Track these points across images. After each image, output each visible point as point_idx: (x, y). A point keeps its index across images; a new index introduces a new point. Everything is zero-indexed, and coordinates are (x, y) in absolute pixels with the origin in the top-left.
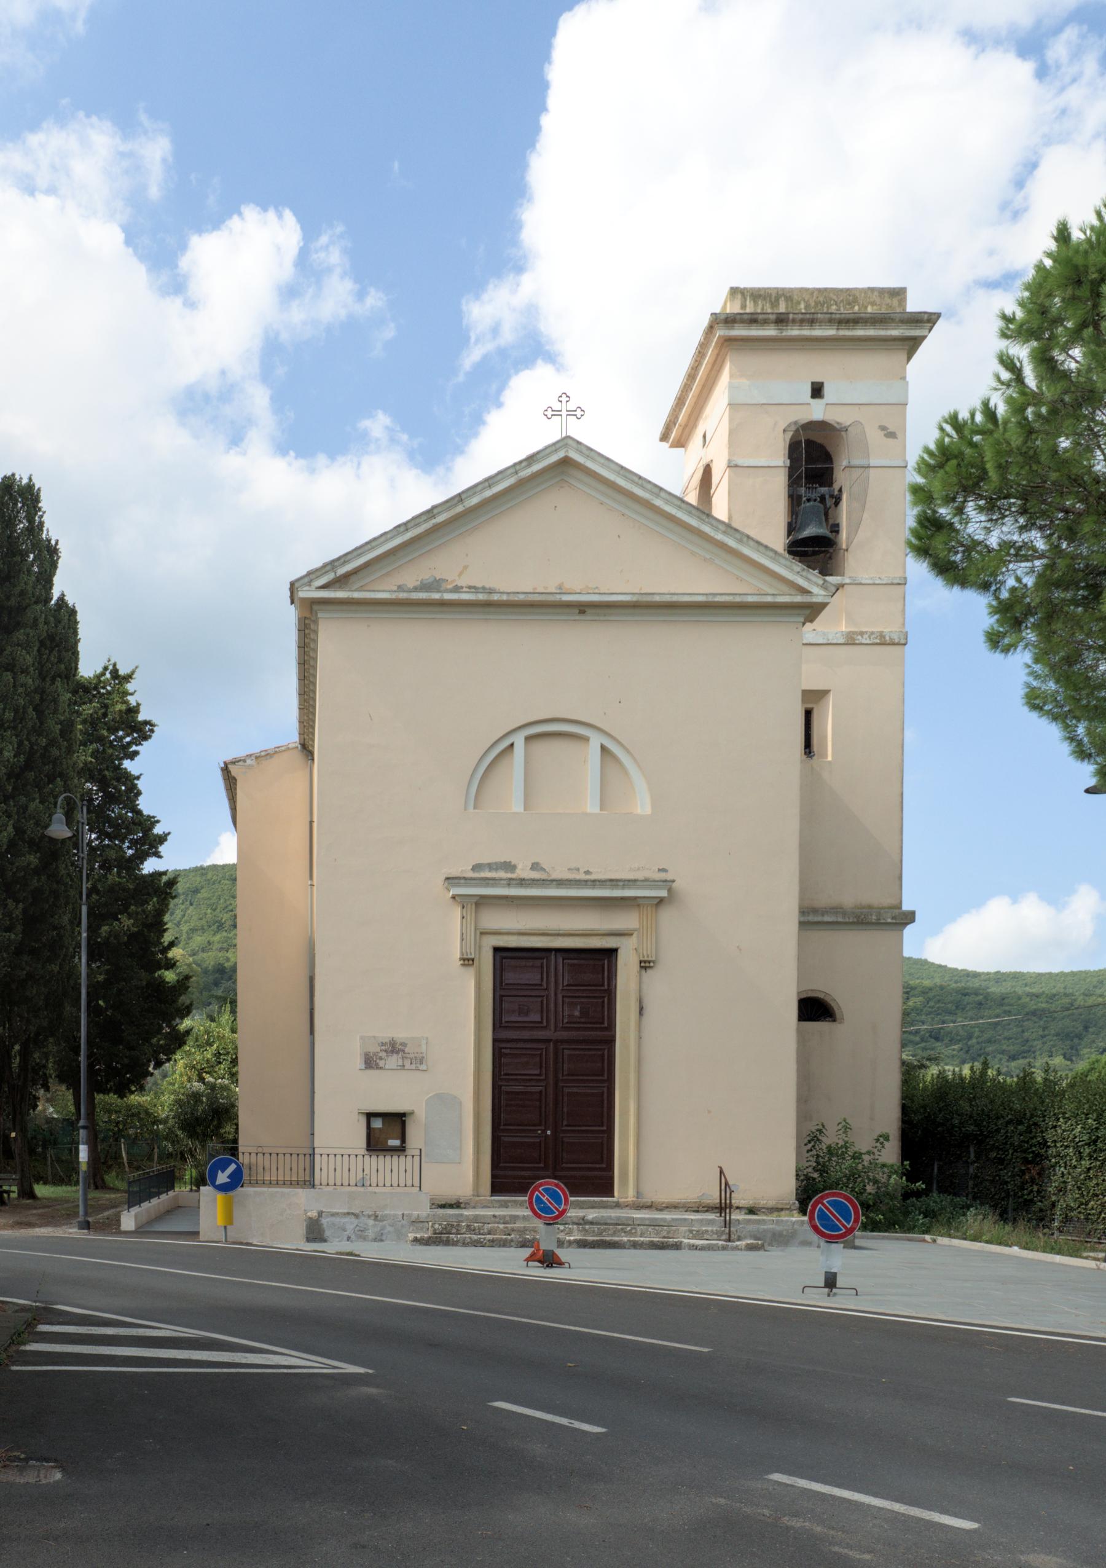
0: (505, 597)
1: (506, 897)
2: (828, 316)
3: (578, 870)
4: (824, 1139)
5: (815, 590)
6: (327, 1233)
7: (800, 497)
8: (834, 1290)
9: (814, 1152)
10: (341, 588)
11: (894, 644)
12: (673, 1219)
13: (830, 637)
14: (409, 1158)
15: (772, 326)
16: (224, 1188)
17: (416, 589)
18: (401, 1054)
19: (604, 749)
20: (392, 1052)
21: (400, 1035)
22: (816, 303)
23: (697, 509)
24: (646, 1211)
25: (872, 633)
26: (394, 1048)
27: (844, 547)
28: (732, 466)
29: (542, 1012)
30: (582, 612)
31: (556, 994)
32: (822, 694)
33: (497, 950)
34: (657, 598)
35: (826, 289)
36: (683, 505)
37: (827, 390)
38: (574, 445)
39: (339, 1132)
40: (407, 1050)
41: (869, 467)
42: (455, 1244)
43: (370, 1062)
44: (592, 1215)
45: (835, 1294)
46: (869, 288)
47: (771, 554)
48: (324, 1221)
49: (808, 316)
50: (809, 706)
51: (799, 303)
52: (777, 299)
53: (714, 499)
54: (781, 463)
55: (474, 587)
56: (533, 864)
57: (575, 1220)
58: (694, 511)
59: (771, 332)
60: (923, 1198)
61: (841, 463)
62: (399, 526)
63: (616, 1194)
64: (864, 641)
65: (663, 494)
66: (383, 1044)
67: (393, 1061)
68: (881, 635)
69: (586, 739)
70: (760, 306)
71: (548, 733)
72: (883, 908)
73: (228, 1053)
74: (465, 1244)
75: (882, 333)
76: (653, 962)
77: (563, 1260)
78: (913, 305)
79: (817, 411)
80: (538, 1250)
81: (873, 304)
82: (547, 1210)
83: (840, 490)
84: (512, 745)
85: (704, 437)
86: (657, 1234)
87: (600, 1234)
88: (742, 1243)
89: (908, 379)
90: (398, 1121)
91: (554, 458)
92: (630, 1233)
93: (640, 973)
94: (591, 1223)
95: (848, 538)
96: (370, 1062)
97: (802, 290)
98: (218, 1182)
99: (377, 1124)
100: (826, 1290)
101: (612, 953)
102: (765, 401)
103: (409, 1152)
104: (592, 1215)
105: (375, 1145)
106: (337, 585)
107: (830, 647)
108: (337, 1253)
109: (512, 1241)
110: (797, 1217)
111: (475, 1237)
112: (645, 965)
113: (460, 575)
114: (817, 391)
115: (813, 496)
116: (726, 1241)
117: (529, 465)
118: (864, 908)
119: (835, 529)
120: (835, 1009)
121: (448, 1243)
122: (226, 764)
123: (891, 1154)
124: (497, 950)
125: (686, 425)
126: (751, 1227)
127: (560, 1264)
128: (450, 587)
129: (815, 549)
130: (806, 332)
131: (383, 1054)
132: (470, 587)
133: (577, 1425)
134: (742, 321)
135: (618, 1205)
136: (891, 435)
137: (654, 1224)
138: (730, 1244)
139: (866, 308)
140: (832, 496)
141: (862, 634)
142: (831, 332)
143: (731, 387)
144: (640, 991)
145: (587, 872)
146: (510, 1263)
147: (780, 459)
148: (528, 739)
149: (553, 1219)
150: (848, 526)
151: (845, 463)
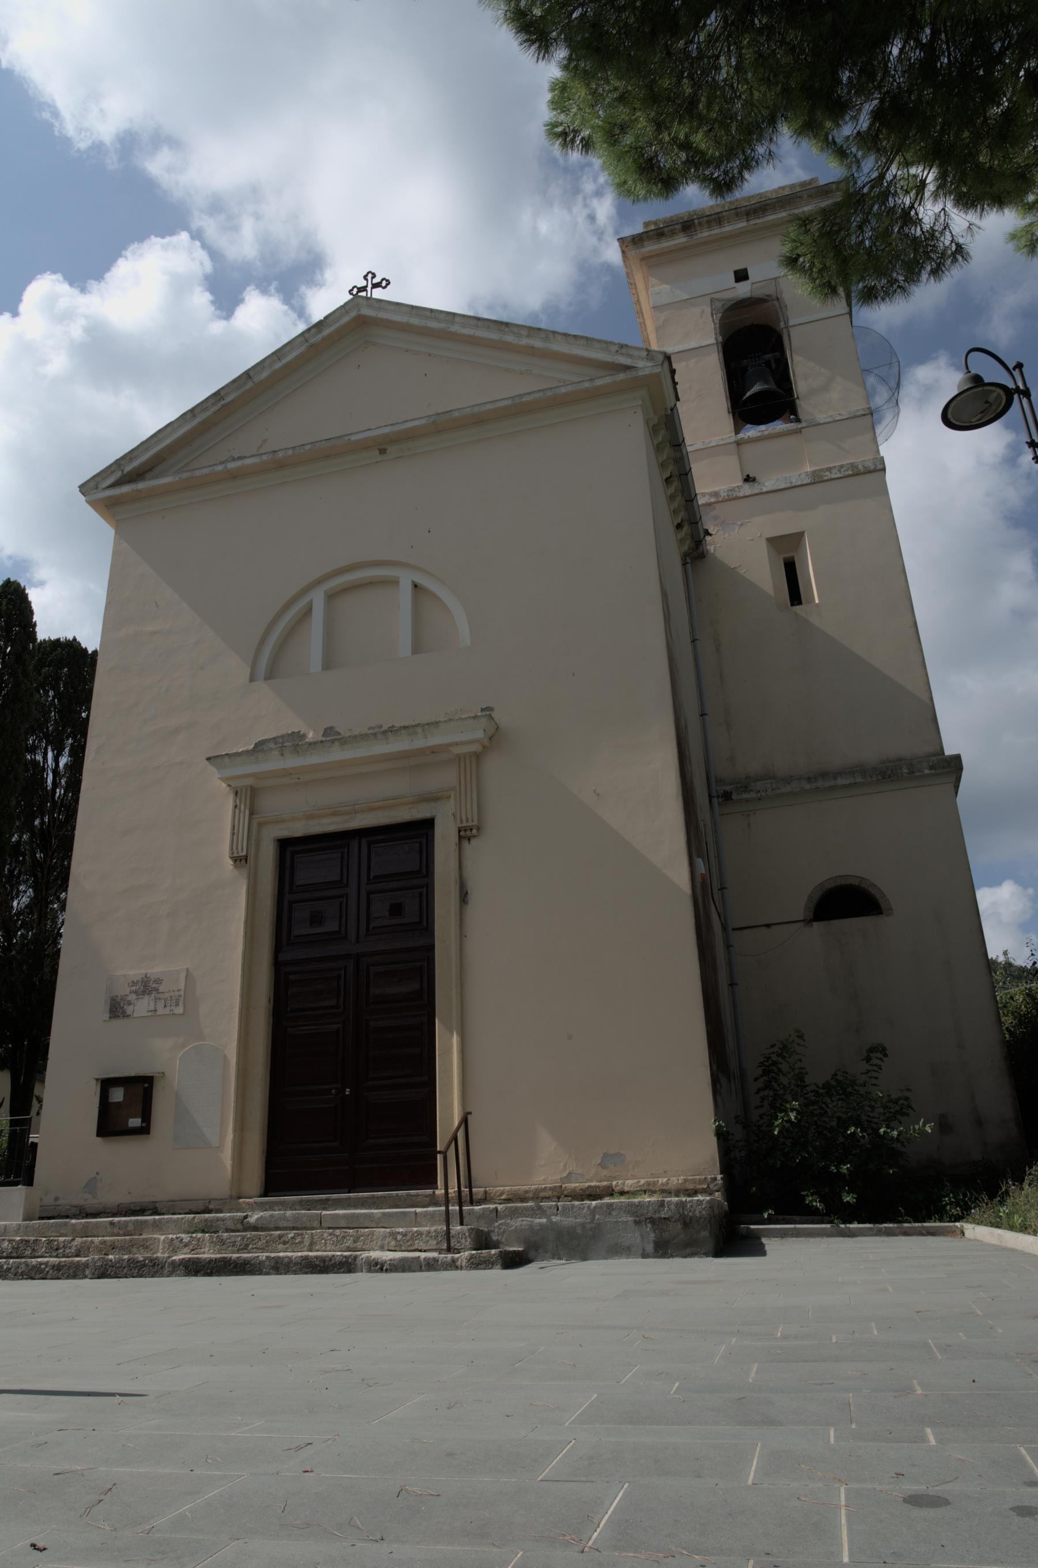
5: (640, 364)
11: (870, 472)
13: (794, 480)
15: (681, 235)
20: (144, 993)
21: (156, 970)
25: (842, 466)
30: (383, 451)
32: (797, 538)
36: (480, 323)
40: (161, 989)
54: (712, 341)
59: (681, 240)
64: (833, 476)
66: (134, 983)
68: (853, 466)
69: (394, 582)
71: (352, 584)
79: (743, 290)
92: (293, 1244)
94: (255, 1228)
99: (117, 1095)
101: (428, 824)
102: (687, 297)
107: (795, 490)
109: (86, 1265)
112: (465, 835)
117: (320, 332)
120: (878, 896)
131: (132, 997)
134: (649, 238)
141: (829, 469)
142: (743, 224)
148: (331, 597)
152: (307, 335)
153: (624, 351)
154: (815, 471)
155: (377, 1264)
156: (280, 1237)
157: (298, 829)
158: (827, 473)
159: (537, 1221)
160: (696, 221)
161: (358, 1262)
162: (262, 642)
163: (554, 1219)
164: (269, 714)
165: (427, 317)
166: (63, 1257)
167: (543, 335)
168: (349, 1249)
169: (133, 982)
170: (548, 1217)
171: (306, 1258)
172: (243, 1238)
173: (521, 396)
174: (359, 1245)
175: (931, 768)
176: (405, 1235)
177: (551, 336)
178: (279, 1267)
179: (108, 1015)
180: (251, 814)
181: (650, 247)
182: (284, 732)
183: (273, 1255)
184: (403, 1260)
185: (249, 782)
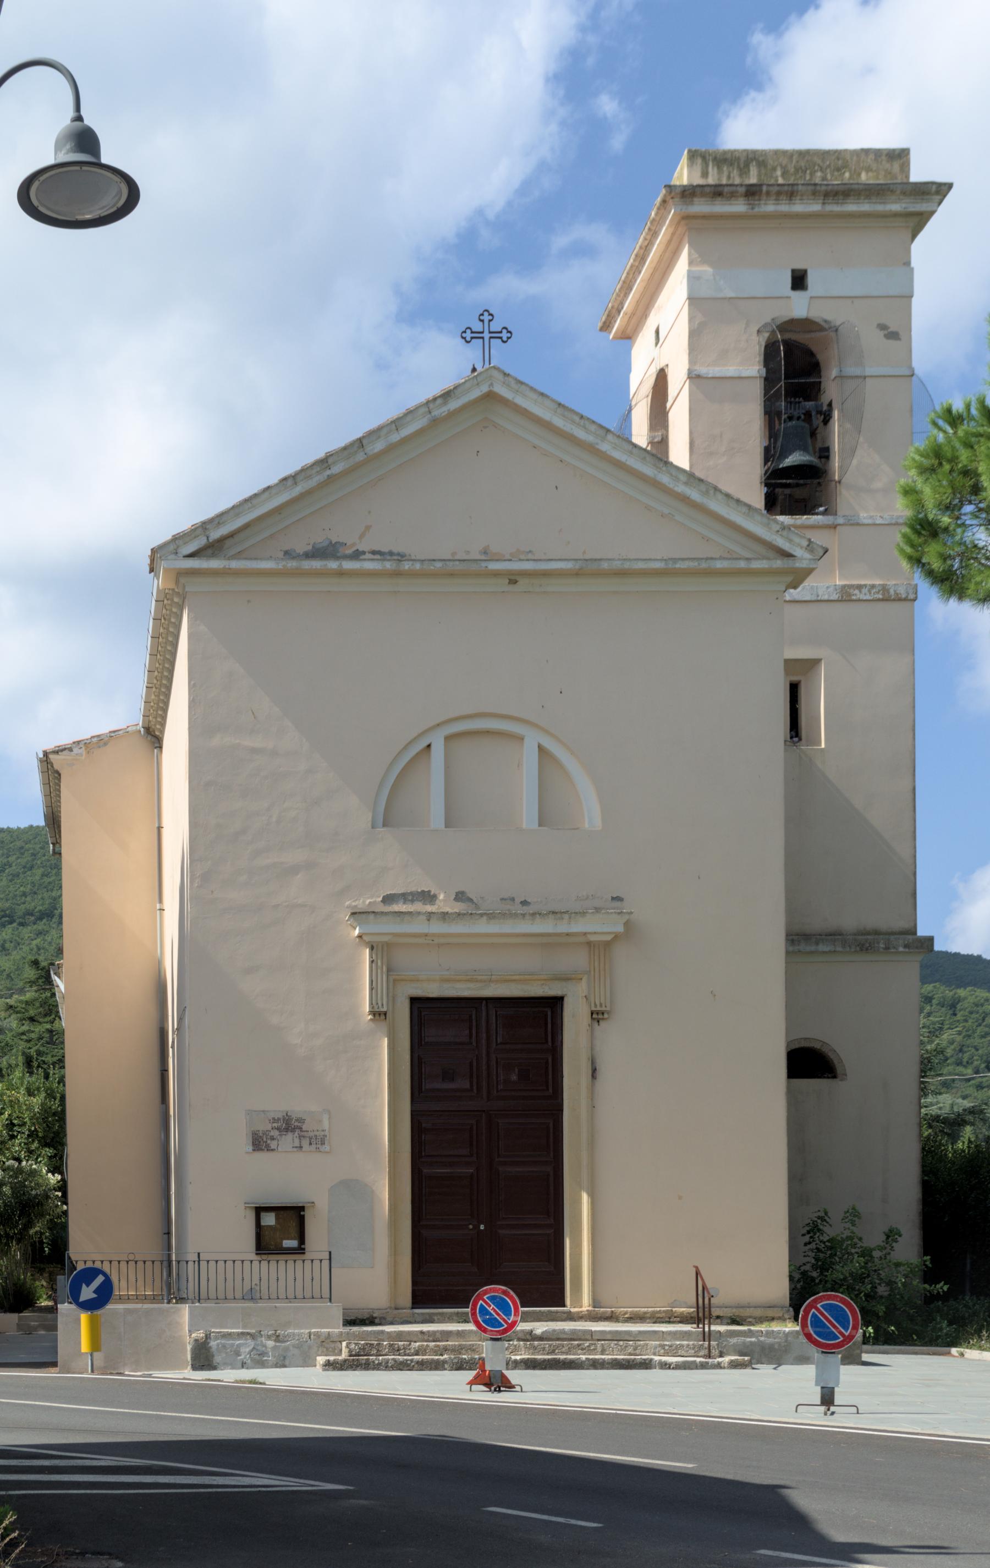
0: (418, 566)
1: (553, 1078)
2: (810, 188)
3: (513, 899)
4: (826, 1229)
5: (798, 552)
6: (218, 1359)
7: (779, 414)
8: (832, 1409)
9: (813, 1246)
10: (213, 556)
11: (900, 600)
12: (640, 1332)
14: (308, 1263)
15: (741, 200)
16: (89, 1306)
17: (308, 556)
18: (297, 1132)
19: (540, 748)
20: (287, 1130)
22: (797, 170)
23: (653, 455)
24: (606, 1323)
25: (873, 586)
26: (289, 1125)
27: (837, 478)
28: (694, 377)
29: (471, 1076)
30: (513, 582)
31: (488, 1054)
33: (414, 1001)
34: (605, 565)
35: (808, 152)
37: (811, 279)
38: (501, 377)
39: (217, 1230)
41: (865, 377)
42: (377, 1367)
43: (259, 1143)
44: (540, 1328)
45: (833, 1413)
46: (862, 150)
47: (744, 509)
48: (213, 1344)
49: (786, 188)
50: (795, 678)
51: (774, 169)
52: (747, 165)
53: (670, 415)
55: (379, 553)
56: (457, 894)
57: (520, 1335)
58: (648, 458)
59: (739, 207)
60: (952, 1302)
61: (831, 373)
62: (285, 479)
63: (568, 1301)
64: (862, 597)
65: (610, 437)
66: (275, 1120)
67: (288, 1140)
68: (884, 588)
69: (521, 739)
70: (726, 174)
71: (475, 734)
72: (893, 933)
73: (24, 1124)
74: (387, 1367)
75: (880, 208)
76: (608, 1013)
77: (513, 1382)
78: (916, 175)
79: (798, 306)
80: (484, 1371)
81: (868, 169)
82: (493, 1322)
83: (830, 405)
84: (429, 746)
85: (657, 332)
86: (623, 1350)
87: (553, 1352)
88: (726, 1359)
89: (913, 265)
90: (294, 1216)
91: (476, 394)
92: (588, 1350)
93: (591, 1026)
95: (840, 467)
96: (259, 1143)
97: (777, 153)
98: (82, 1299)
99: (269, 1220)
100: (823, 1408)
101: (556, 1003)
102: (732, 295)
103: (308, 1255)
104: (540, 1328)
105: (265, 1245)
106: (210, 551)
108: (236, 1382)
109: (444, 1362)
110: (791, 1327)
111: (401, 1358)
112: (597, 1016)
113: (362, 536)
114: (799, 281)
115: (796, 414)
116: (703, 1357)
117: (445, 403)
118: (868, 933)
119: (825, 453)
120: (836, 1062)
121: (367, 1366)
122: (46, 754)
123: (909, 1250)
124: (414, 1001)
125: (633, 314)
126: (734, 1341)
127: (509, 1386)
128: (349, 552)
129: (797, 484)
130: (784, 208)
131: (275, 1133)
132: (374, 553)
133: (573, 1522)
134: (703, 195)
135: (571, 1317)
136: (893, 336)
137: (617, 1337)
138: (710, 1360)
139: (859, 174)
140: (820, 412)
141: (860, 587)
142: (816, 207)
143: (693, 278)
144: (592, 1048)
145: (524, 903)
146: (452, 1386)
147: (754, 369)
148: (448, 738)
149: (502, 1333)
150: (842, 450)
151: (834, 373)
152: (431, 406)
153: (785, 533)
154: (844, 587)
155: (666, 1364)
156: (579, 1345)
157: (433, 990)
158: (857, 592)
159: (749, 1340)
160: (764, 188)
161: (653, 1363)
162: (381, 785)
163: (762, 1339)
164: (393, 866)
165: (573, 422)
166: (405, 1355)
167: (703, 487)
168: (630, 1354)
169: (274, 1119)
170: (757, 1337)
171: (616, 1359)
172: (550, 1346)
173: (675, 560)
174: (638, 1352)
175: (906, 946)
176: (671, 1346)
177: (712, 492)
178: (596, 1365)
179: (251, 1148)
180: (389, 970)
181: (700, 207)
182: (414, 889)
183: (591, 1357)
184: (685, 1362)
185: (386, 939)
